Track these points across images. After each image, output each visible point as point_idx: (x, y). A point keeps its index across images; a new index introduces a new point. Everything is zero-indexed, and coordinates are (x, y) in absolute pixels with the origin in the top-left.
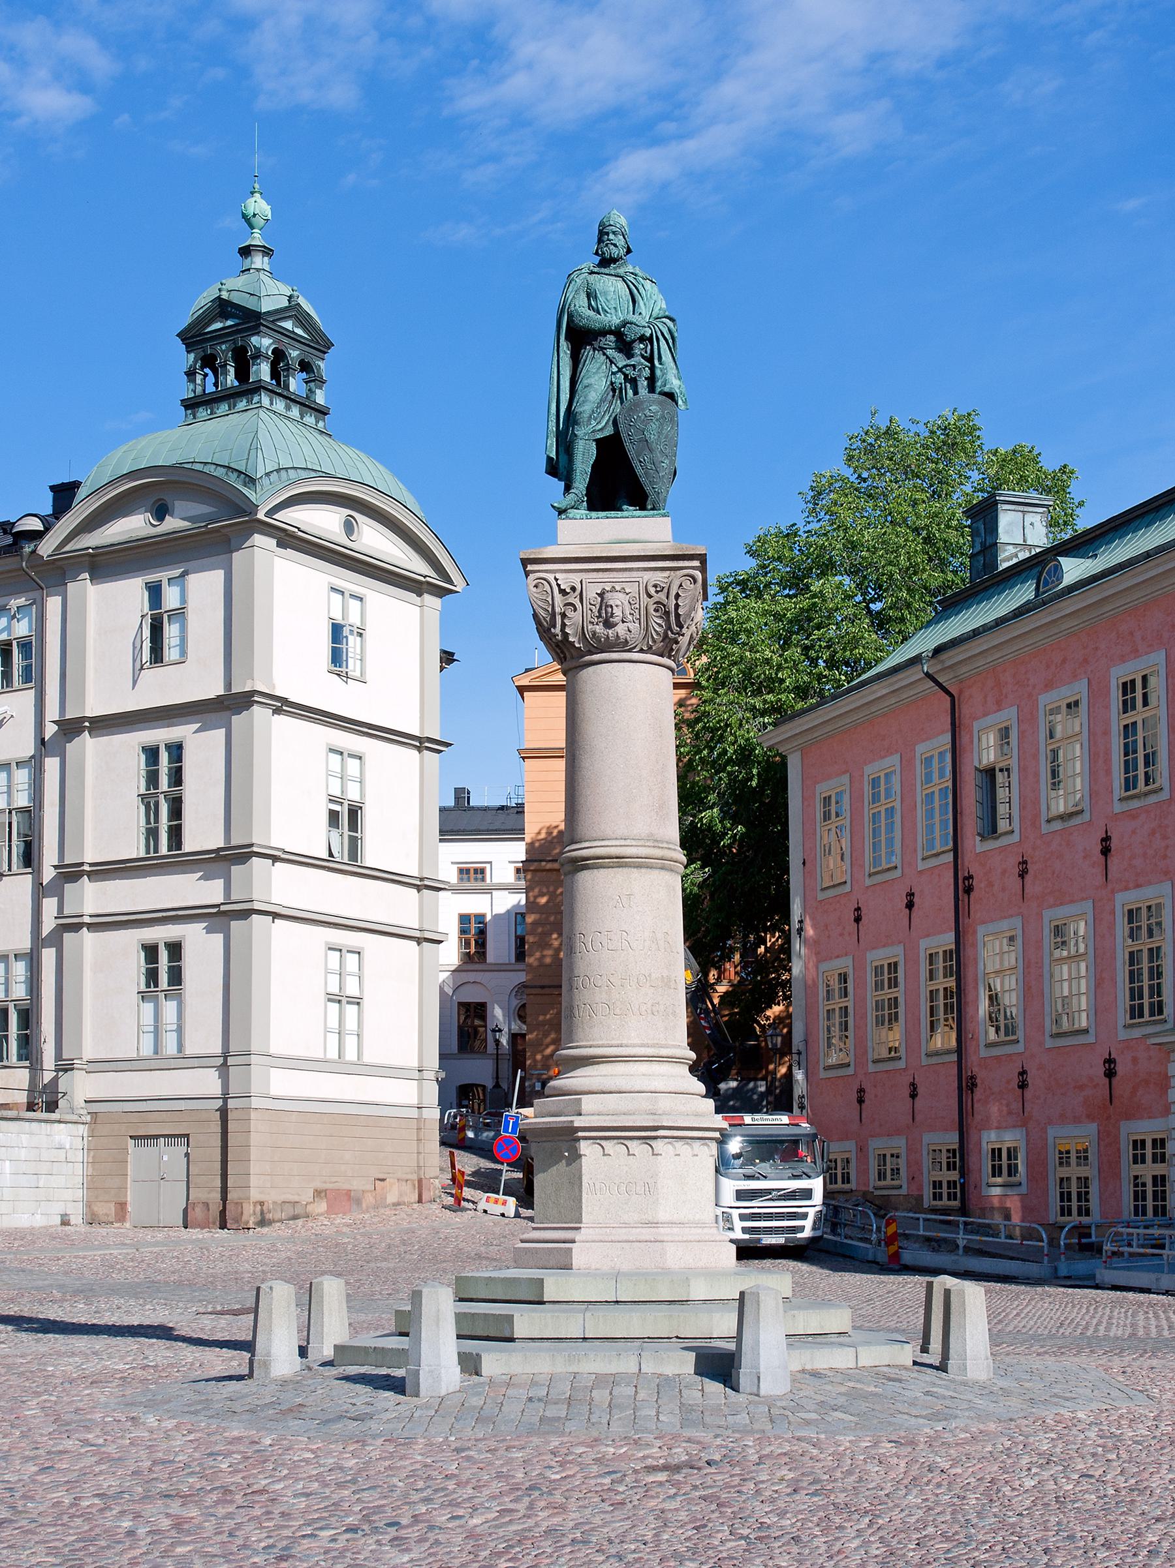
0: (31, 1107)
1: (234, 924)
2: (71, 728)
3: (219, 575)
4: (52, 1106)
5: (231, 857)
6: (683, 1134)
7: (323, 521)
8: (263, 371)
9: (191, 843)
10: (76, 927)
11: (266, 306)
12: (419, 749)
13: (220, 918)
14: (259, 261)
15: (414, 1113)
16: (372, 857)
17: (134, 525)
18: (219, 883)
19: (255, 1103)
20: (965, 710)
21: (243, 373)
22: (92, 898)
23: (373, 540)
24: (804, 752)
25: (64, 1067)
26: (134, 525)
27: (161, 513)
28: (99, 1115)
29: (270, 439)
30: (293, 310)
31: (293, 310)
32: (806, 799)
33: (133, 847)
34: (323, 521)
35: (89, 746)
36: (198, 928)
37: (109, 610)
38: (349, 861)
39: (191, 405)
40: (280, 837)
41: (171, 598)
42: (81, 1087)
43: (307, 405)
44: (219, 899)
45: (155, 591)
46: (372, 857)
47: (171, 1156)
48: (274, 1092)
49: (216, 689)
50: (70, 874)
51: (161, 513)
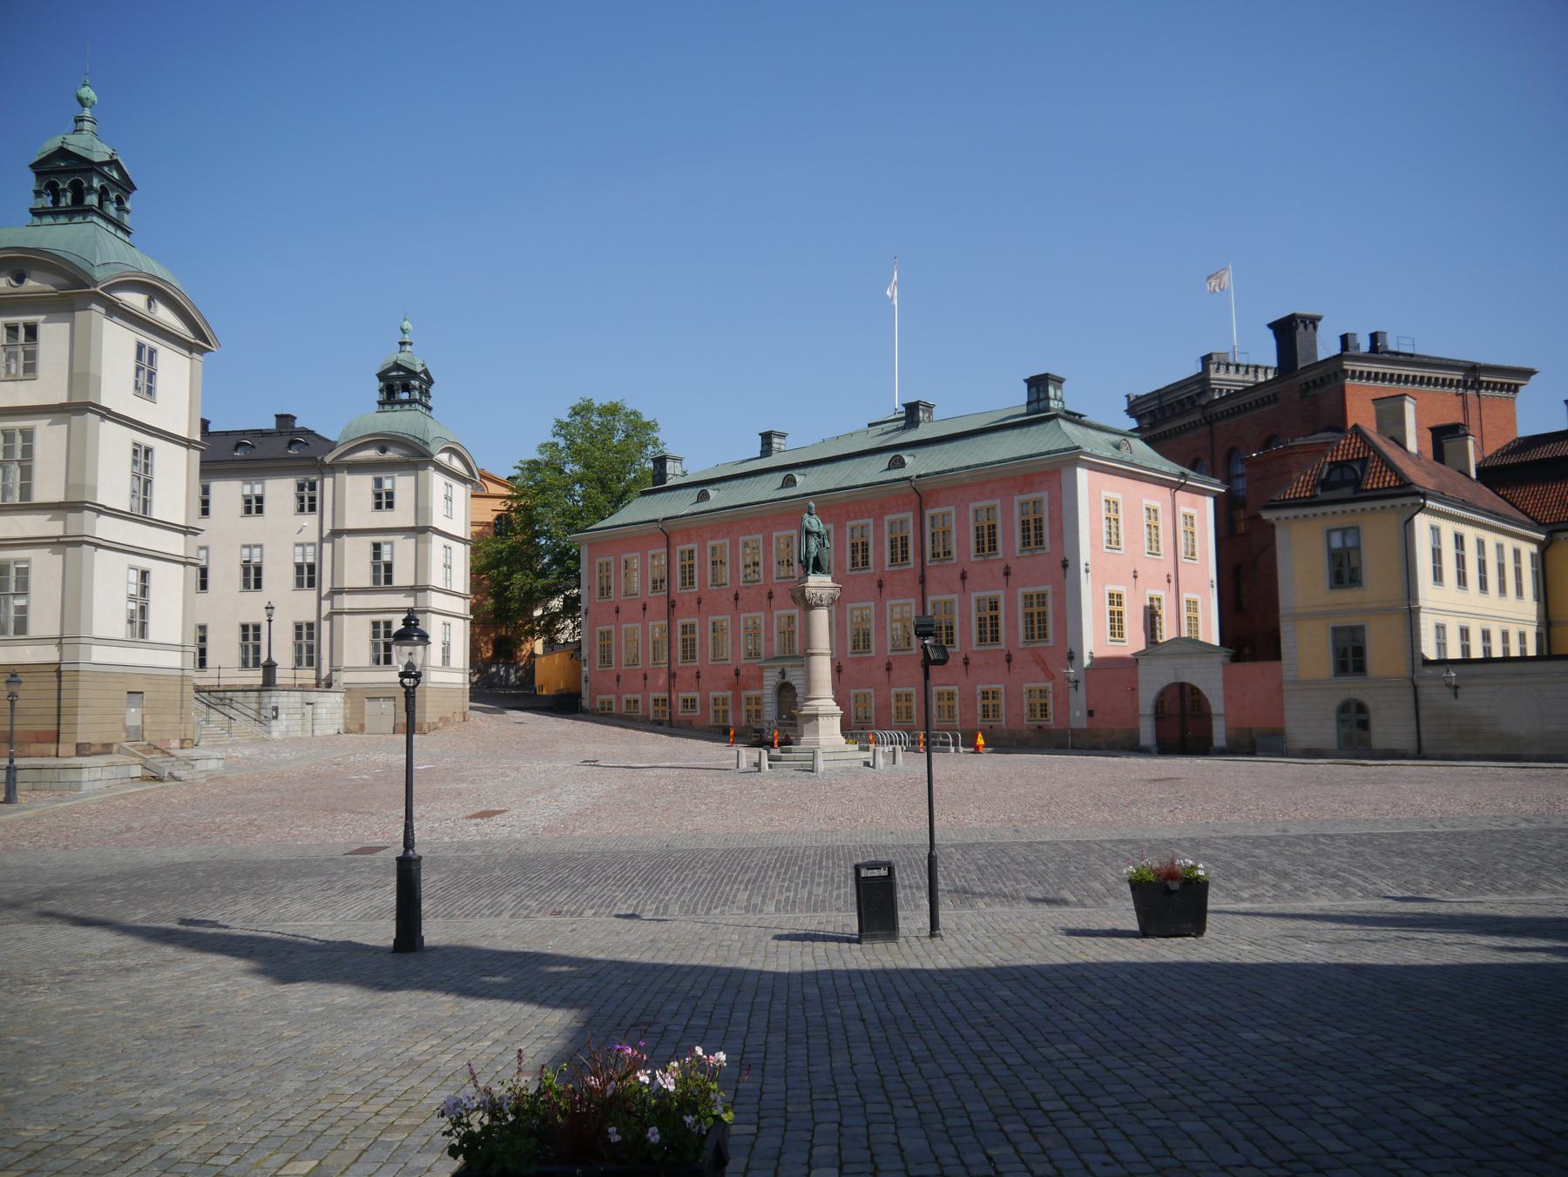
0: (317, 685)
1: (69, 550)
2: (337, 533)
3: (412, 479)
4: (329, 685)
5: (418, 589)
6: (832, 715)
7: (135, 300)
8: (92, 200)
9: (396, 582)
10: (341, 613)
11: (97, 158)
12: (188, 447)
13: (59, 544)
14: (87, 126)
15: (179, 673)
16: (157, 513)
17: (371, 454)
18: (60, 524)
19: (82, 667)
20: (672, 541)
21: (78, 198)
22: (348, 602)
23: (391, 454)
24: (590, 546)
25: (334, 669)
26: (371, 454)
27: (383, 450)
28: (349, 691)
29: (87, 241)
30: (113, 163)
31: (113, 163)
32: (591, 563)
33: (367, 582)
34: (135, 300)
35: (347, 540)
36: (44, 553)
37: (358, 488)
38: (141, 515)
39: (36, 213)
40: (103, 498)
41: (387, 485)
42: (345, 678)
43: (119, 225)
44: (61, 533)
45: (378, 482)
46: (157, 513)
47: (387, 706)
48: (94, 660)
49: (61, 397)
50: (336, 591)
51: (383, 450)
